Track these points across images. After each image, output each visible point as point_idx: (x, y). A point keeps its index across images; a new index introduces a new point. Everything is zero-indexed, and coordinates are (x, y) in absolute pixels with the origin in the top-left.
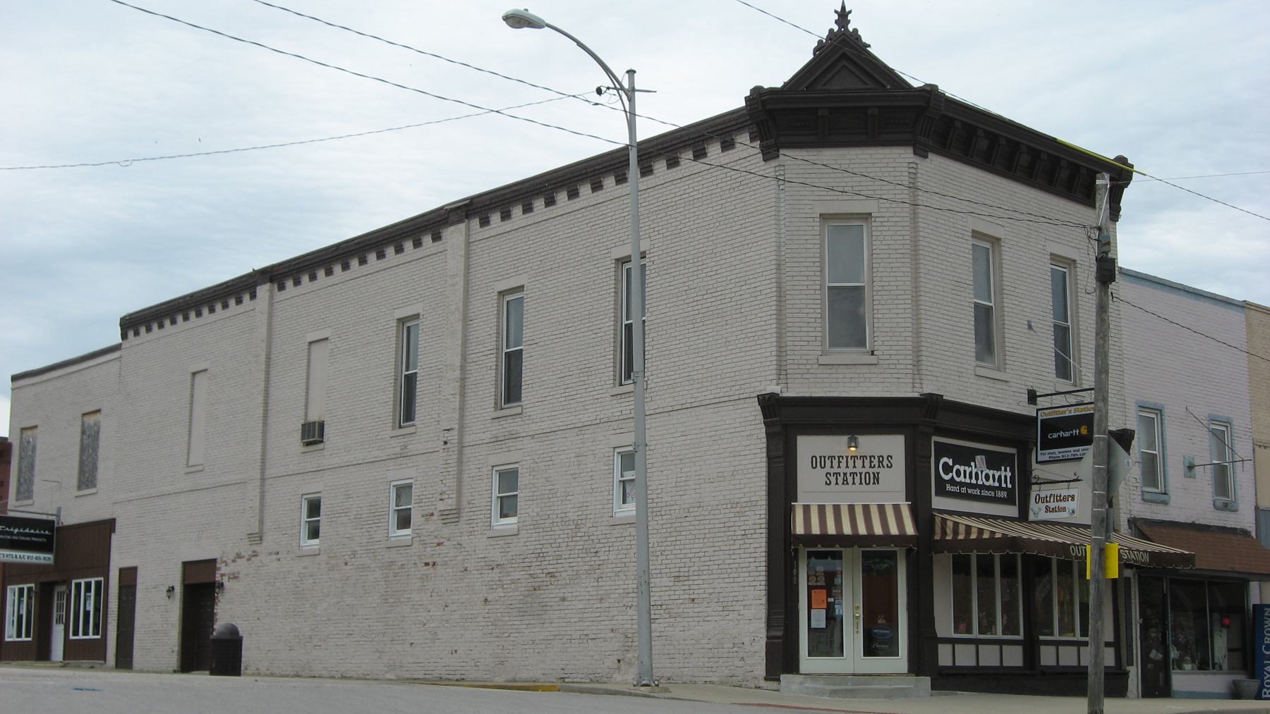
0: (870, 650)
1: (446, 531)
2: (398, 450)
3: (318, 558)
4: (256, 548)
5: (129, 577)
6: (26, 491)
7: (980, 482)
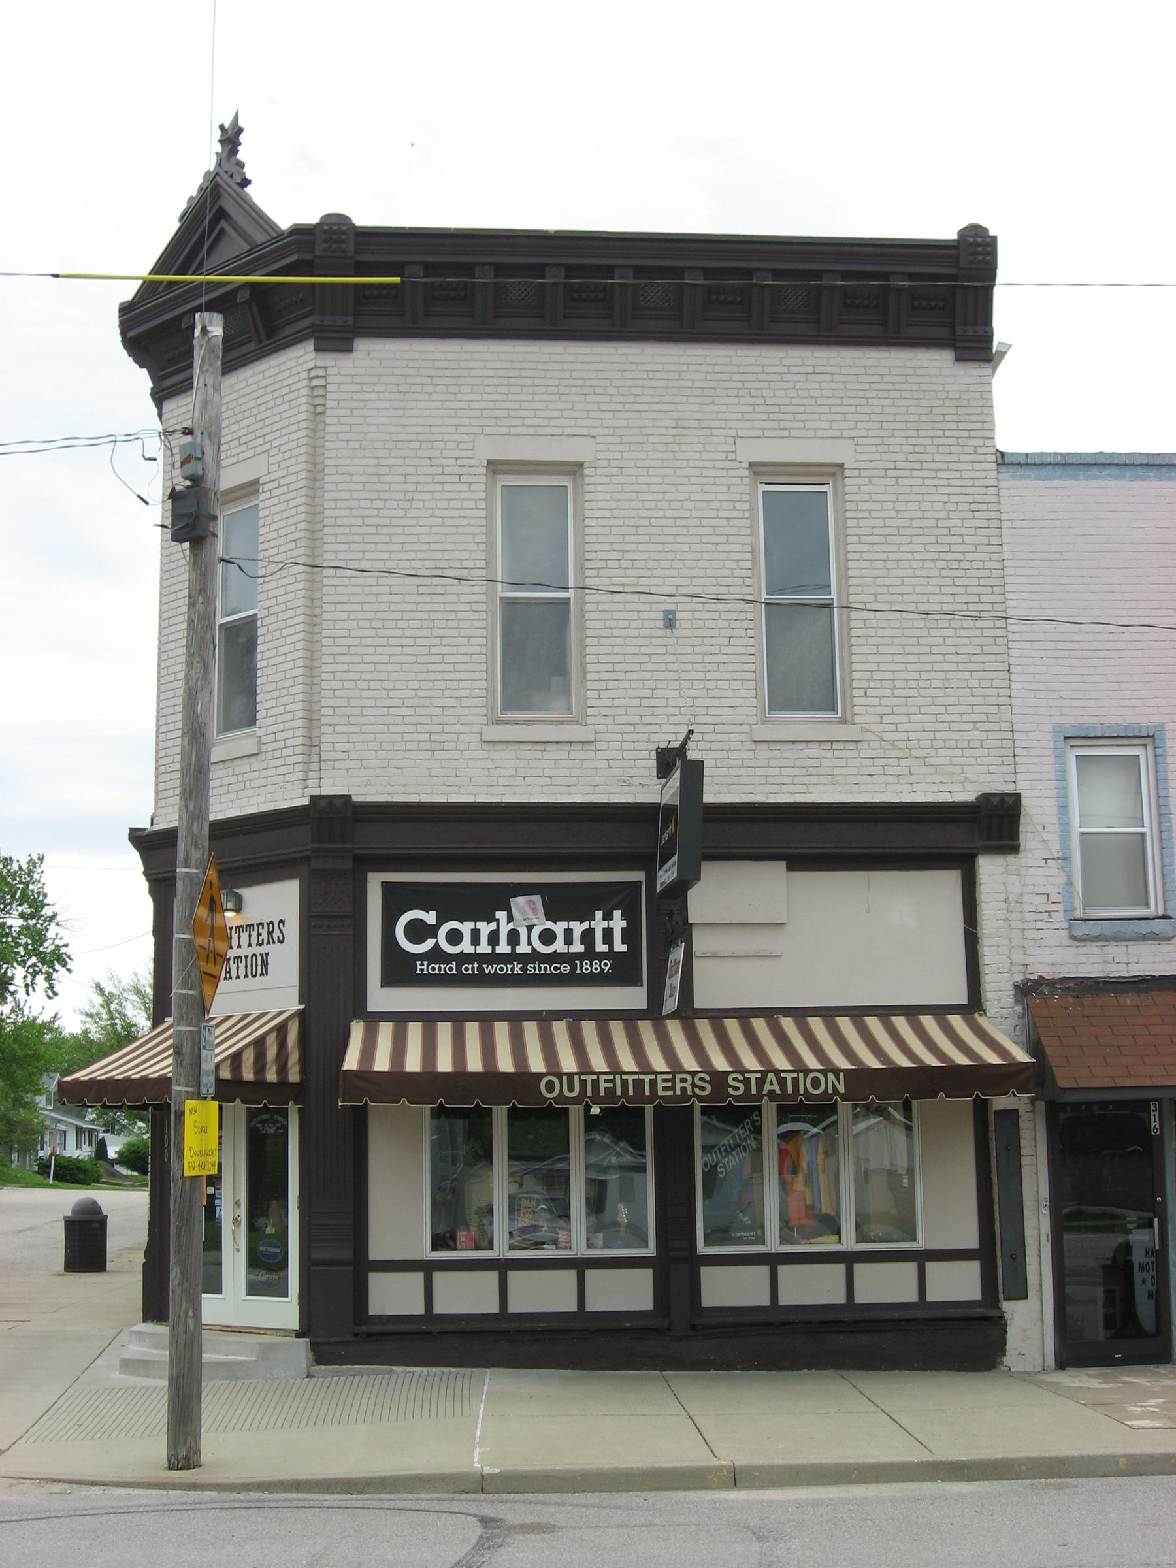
0: (254, 1289)
7: (523, 948)
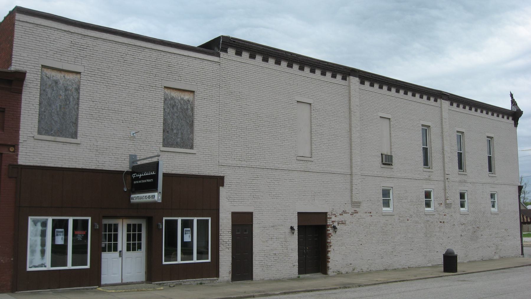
1: (447, 211)
2: (427, 177)
3: (393, 217)
4: (356, 209)
5: (243, 223)
6: (61, 121)
